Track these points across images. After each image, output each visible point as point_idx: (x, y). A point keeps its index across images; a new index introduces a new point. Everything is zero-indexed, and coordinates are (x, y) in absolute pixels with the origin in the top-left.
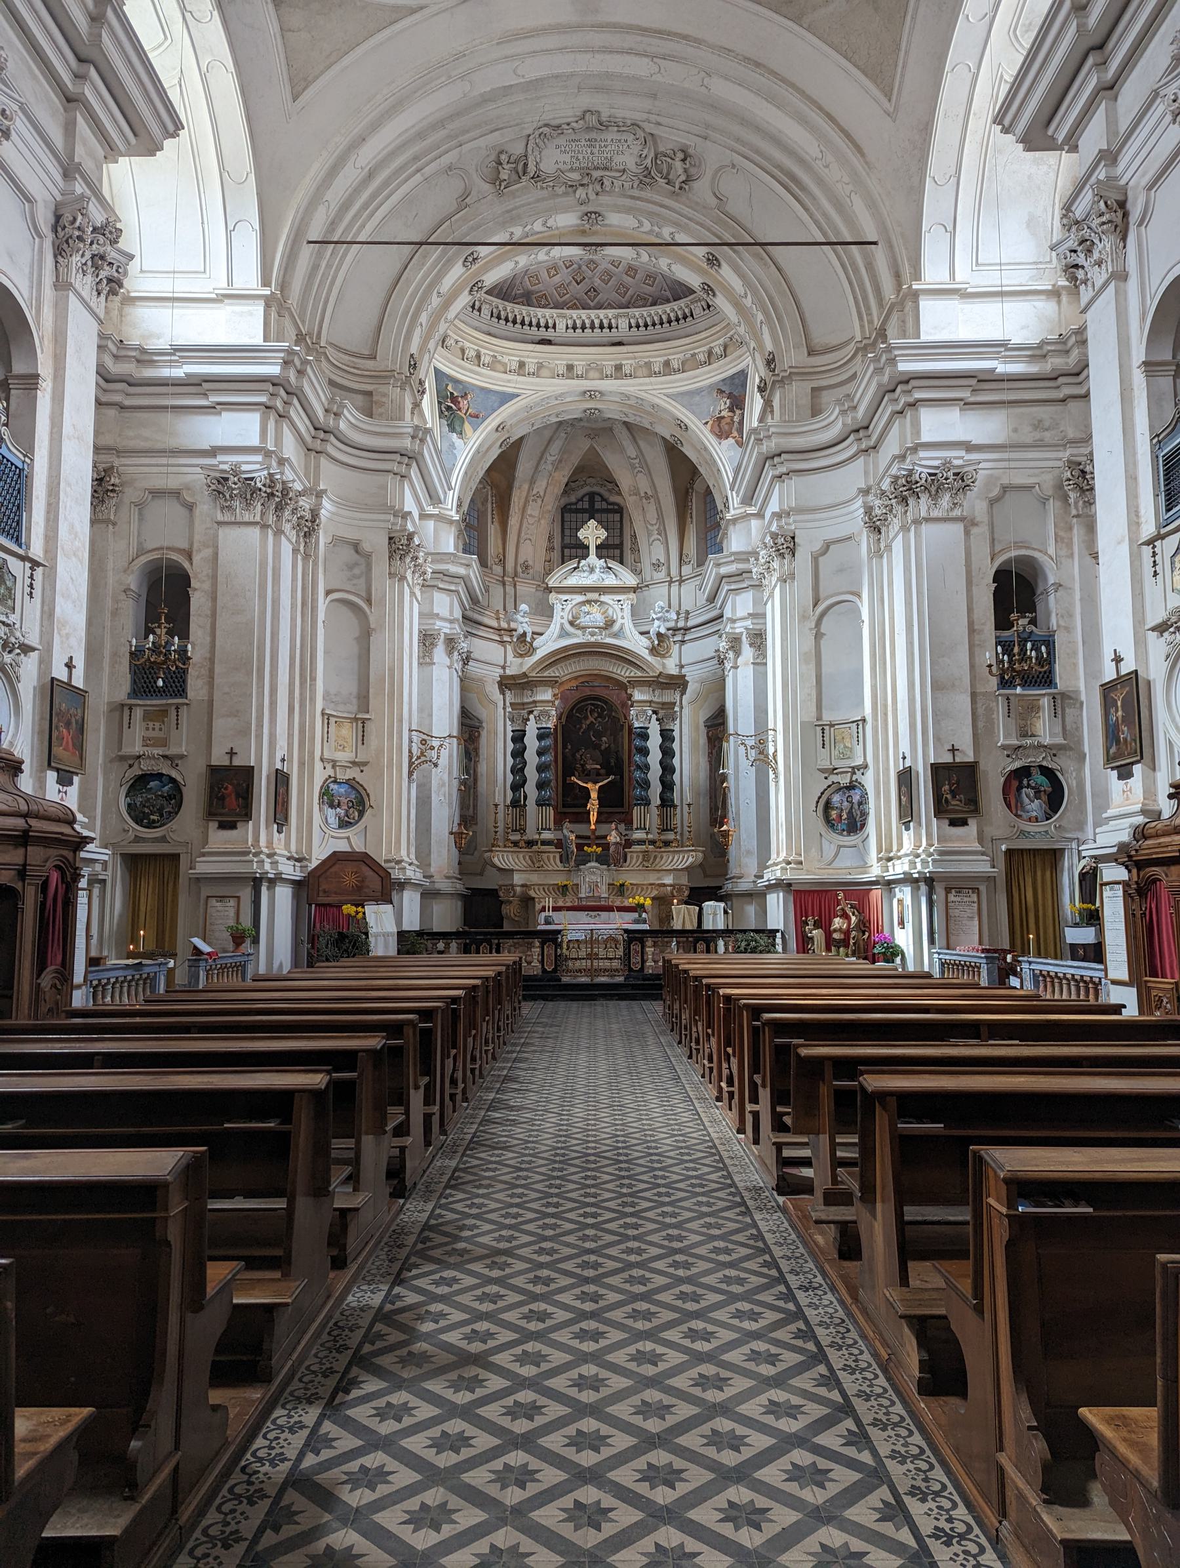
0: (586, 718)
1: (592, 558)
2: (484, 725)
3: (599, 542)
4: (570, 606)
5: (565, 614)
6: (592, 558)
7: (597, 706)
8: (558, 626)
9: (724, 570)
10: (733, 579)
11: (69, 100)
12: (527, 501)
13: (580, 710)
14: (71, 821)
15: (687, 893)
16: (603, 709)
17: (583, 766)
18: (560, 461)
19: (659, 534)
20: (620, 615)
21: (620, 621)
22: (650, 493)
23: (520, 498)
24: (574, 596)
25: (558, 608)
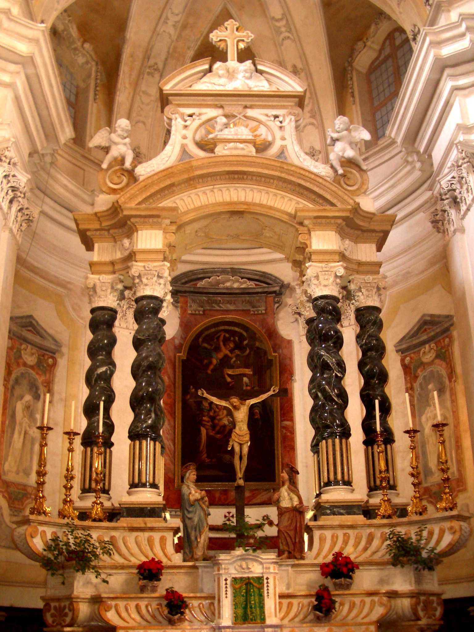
0: (217, 349)
1: (232, 63)
2: (64, 350)
3: (242, 46)
4: (197, 123)
5: (189, 133)
6: (232, 63)
7: (233, 333)
8: (177, 149)
9: (447, 51)
10: (460, 70)
11: (31, 324)
12: (140, 74)
13: (209, 339)
14: (335, 584)
15: (438, 612)
16: (241, 336)
17: (213, 419)
18: (184, 27)
19: (313, 117)
20: (278, 134)
21: (278, 144)
22: (299, 66)
23: (131, 69)
24: (204, 110)
25: (177, 124)
